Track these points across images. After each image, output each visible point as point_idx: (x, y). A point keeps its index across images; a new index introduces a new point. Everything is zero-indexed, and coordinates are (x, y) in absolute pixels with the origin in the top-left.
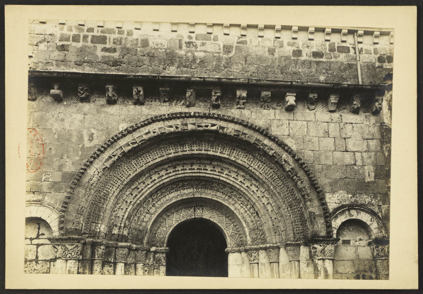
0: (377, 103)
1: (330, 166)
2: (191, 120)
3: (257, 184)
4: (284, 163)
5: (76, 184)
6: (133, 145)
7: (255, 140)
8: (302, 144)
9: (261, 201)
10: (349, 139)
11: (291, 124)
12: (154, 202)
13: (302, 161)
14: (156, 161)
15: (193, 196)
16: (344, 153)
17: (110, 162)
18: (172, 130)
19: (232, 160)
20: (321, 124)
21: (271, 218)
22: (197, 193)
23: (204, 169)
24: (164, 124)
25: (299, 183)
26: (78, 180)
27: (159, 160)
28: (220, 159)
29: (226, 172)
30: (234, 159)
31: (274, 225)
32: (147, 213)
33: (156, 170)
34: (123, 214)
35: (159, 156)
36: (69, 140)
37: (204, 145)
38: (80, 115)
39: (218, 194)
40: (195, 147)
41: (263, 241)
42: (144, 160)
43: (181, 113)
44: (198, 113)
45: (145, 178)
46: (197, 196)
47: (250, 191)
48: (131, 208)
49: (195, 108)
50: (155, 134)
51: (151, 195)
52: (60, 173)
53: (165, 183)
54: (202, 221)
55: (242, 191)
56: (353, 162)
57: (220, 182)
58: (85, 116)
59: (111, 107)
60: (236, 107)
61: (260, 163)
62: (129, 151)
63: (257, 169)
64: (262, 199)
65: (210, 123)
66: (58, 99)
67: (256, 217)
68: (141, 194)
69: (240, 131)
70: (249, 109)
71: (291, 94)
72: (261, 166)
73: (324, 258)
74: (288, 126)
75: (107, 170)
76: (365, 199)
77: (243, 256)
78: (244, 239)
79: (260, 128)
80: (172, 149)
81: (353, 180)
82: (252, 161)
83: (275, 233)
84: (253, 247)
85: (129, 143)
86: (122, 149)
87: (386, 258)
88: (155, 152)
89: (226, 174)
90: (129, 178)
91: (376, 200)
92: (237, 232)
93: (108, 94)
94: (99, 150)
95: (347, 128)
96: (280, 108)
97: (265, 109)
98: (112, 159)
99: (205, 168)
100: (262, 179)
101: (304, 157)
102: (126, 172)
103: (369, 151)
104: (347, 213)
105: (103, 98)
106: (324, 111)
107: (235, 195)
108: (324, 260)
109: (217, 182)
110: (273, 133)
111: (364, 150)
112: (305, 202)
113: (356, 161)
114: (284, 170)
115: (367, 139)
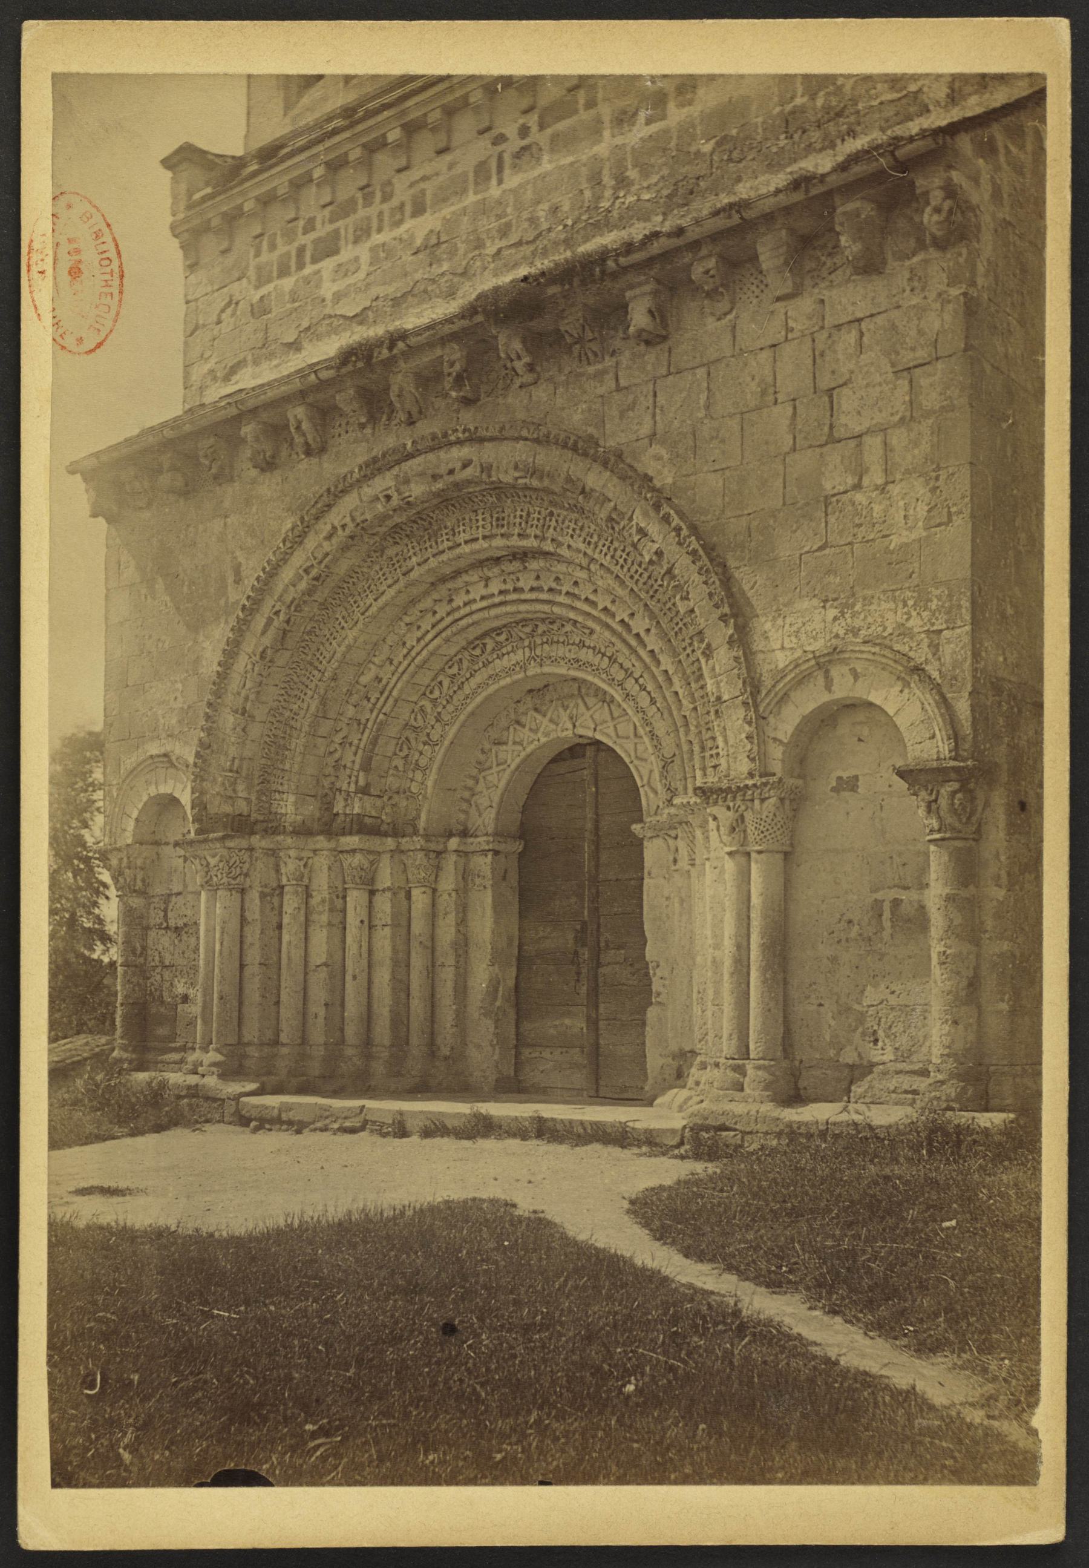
10: (845, 391)
16: (825, 449)
17: (271, 633)
32: (425, 744)
91: (925, 614)
101: (694, 501)
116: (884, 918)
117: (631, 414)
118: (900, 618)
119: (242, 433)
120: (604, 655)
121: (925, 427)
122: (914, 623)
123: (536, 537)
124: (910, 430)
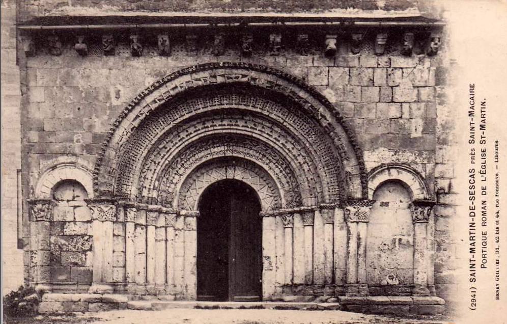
0: (433, 43)
1: (372, 120)
2: (220, 72)
3: (293, 141)
4: (320, 117)
5: (106, 146)
6: (160, 101)
7: (290, 92)
8: (342, 95)
9: (297, 160)
10: (397, 88)
11: (330, 72)
12: (183, 162)
13: (341, 116)
14: (185, 117)
15: (223, 155)
18: (200, 83)
19: (265, 115)
20: (365, 70)
21: (307, 178)
22: (228, 152)
23: (235, 125)
24: (191, 76)
25: (336, 139)
26: (108, 141)
27: (187, 116)
28: (254, 114)
29: (259, 128)
30: (267, 114)
31: (309, 187)
32: (176, 174)
33: (184, 127)
34: (152, 176)
35: (187, 112)
36: (96, 98)
37: (235, 97)
38: (105, 70)
39: (251, 152)
40: (225, 101)
41: (298, 204)
42: (172, 117)
43: (209, 64)
44: (228, 63)
45: (172, 136)
46: (229, 155)
47: (285, 149)
48: (160, 169)
49: (224, 57)
50: (183, 89)
51: (179, 154)
52: (90, 135)
53: (194, 141)
54: (233, 182)
55: (276, 149)
56: (398, 115)
57: (253, 139)
58: (111, 71)
59: (136, 60)
60: (269, 54)
61: (296, 118)
62: (157, 109)
63: (292, 125)
64: (298, 158)
65: (241, 73)
66: (82, 54)
67: (292, 177)
68: (169, 153)
69: (273, 83)
70: (284, 56)
71: (332, 37)
72: (297, 121)
73: (358, 220)
74: (327, 75)
75: (136, 130)
76: (407, 157)
77: (277, 221)
78: (280, 202)
79: (295, 78)
80: (201, 104)
81: (397, 135)
82: (287, 116)
83: (311, 195)
84: (287, 210)
85: (156, 100)
86: (149, 106)
87: (425, 221)
88: (183, 108)
89: (259, 130)
90: (156, 137)
92: (272, 195)
93: (133, 47)
94: (127, 109)
95: (395, 75)
96: (319, 52)
97: (302, 55)
98: (140, 118)
99: (236, 124)
100: (297, 136)
101: (343, 110)
102: (154, 131)
103: (419, 102)
104: (387, 172)
105: (127, 49)
106: (371, 54)
107: (270, 153)
108: (357, 223)
109: (250, 139)
110: (310, 84)
111: (413, 100)
112: (342, 161)
113: (402, 113)
114: (321, 125)
115: (418, 87)
116: (396, 244)
117: (319, 76)
118: (414, 158)
119: (131, 37)
120: (260, 153)
121: (423, 105)
122: (418, 160)
123: (260, 108)
124: (417, 105)
